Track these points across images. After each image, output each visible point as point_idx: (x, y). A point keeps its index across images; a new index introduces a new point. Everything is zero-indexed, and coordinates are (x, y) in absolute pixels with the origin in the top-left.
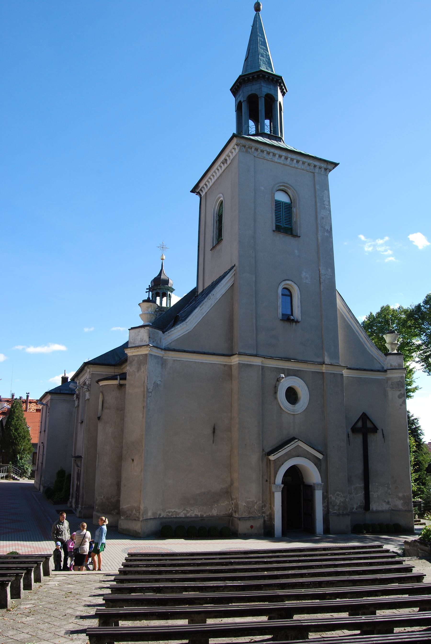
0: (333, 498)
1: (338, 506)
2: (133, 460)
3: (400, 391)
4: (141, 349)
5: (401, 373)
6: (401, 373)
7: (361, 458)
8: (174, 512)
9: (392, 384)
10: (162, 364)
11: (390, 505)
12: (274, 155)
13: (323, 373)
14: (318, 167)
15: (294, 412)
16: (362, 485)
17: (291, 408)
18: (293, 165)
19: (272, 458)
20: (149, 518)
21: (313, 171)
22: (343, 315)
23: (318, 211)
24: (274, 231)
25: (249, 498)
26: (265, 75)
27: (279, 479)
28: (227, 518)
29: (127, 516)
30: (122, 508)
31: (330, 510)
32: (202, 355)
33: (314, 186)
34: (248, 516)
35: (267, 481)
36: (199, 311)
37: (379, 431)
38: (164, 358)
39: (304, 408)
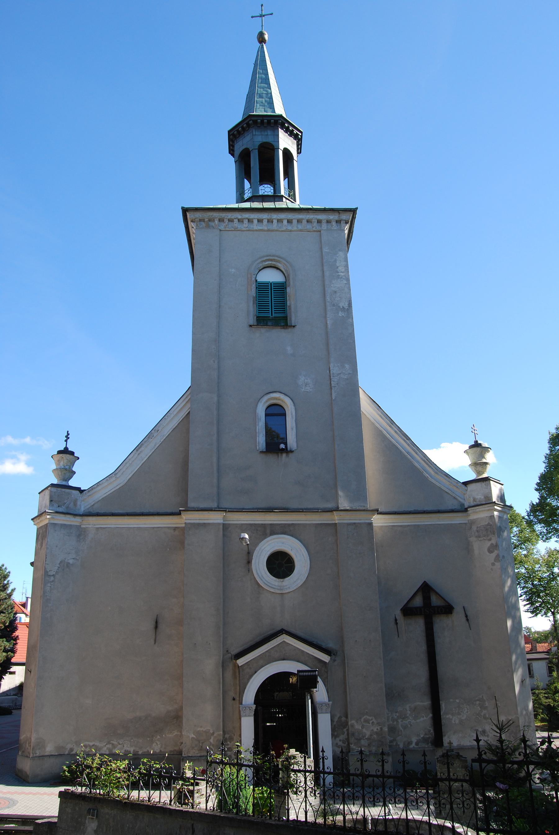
0: (358, 727)
1: (368, 739)
3: (490, 540)
5: (488, 510)
6: (488, 510)
7: (424, 657)
8: (93, 745)
9: (477, 531)
10: (79, 536)
11: (488, 736)
12: (250, 221)
13: (335, 524)
14: (324, 221)
15: (281, 589)
16: (427, 703)
17: (277, 584)
18: (284, 228)
19: (241, 662)
20: (46, 754)
21: (318, 228)
22: (381, 431)
23: (327, 282)
24: (251, 326)
25: (201, 727)
26: (270, 120)
27: (249, 696)
28: (177, 756)
31: (352, 746)
32: (137, 517)
33: (321, 249)
34: (199, 755)
35: (234, 699)
36: (136, 455)
37: (458, 609)
38: (83, 526)
39: (300, 583)
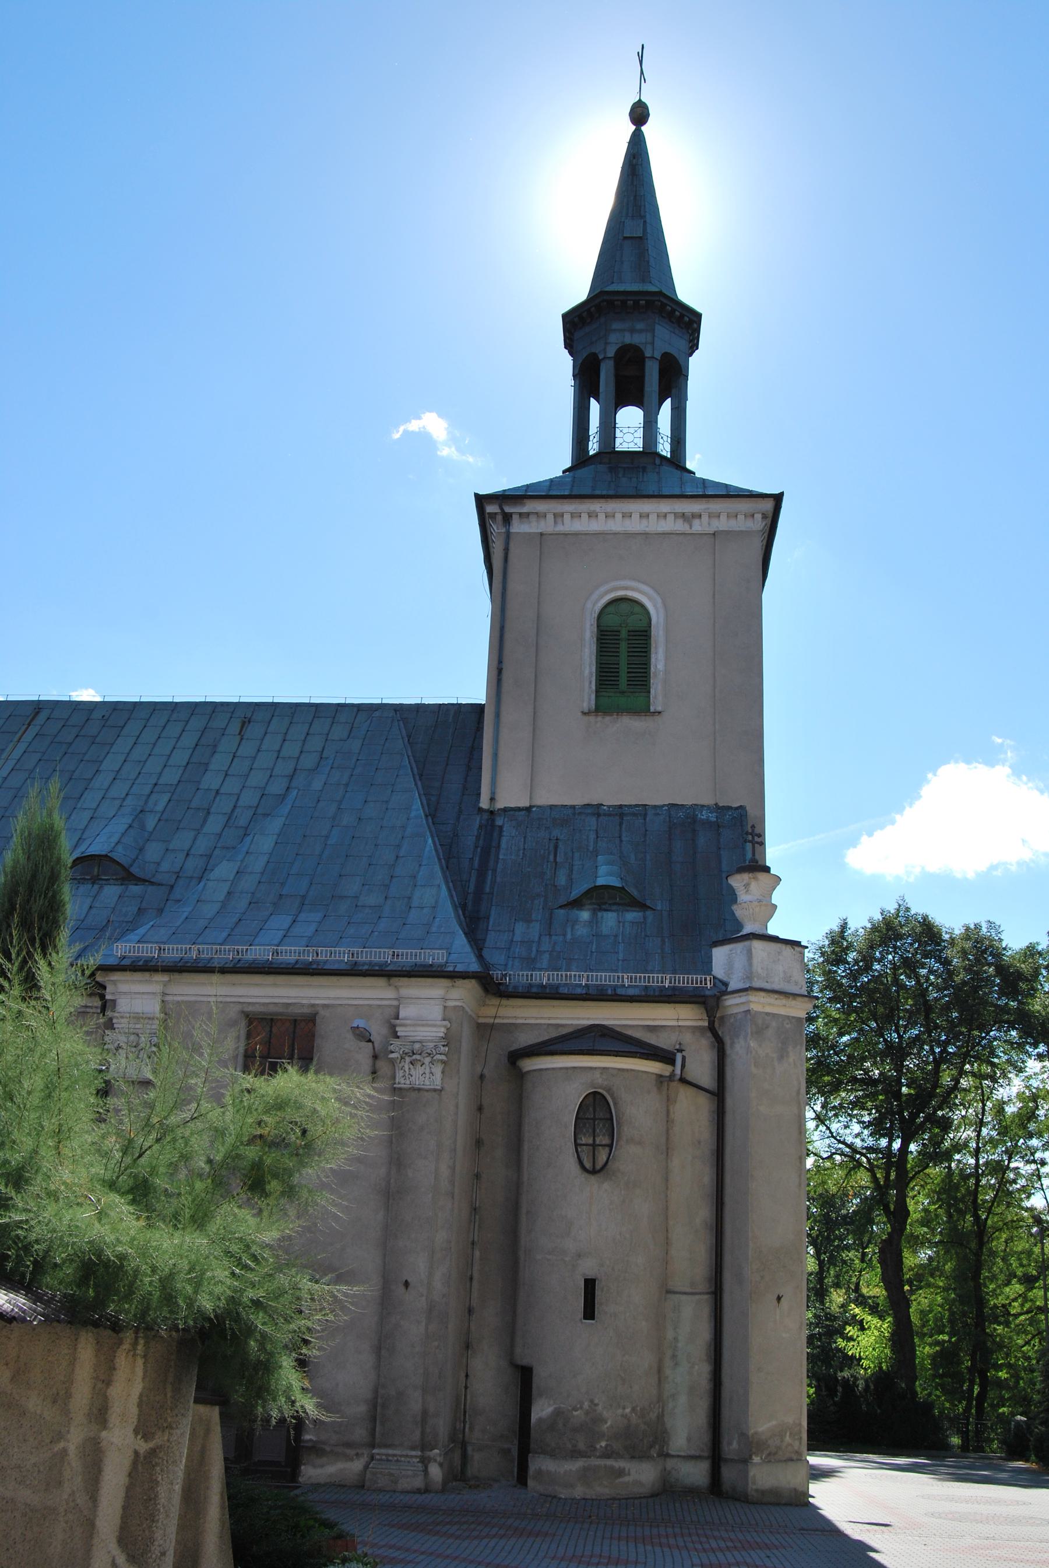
2: (779, 1298)
4: (794, 1002)
29: (769, 1454)
30: (756, 1433)
